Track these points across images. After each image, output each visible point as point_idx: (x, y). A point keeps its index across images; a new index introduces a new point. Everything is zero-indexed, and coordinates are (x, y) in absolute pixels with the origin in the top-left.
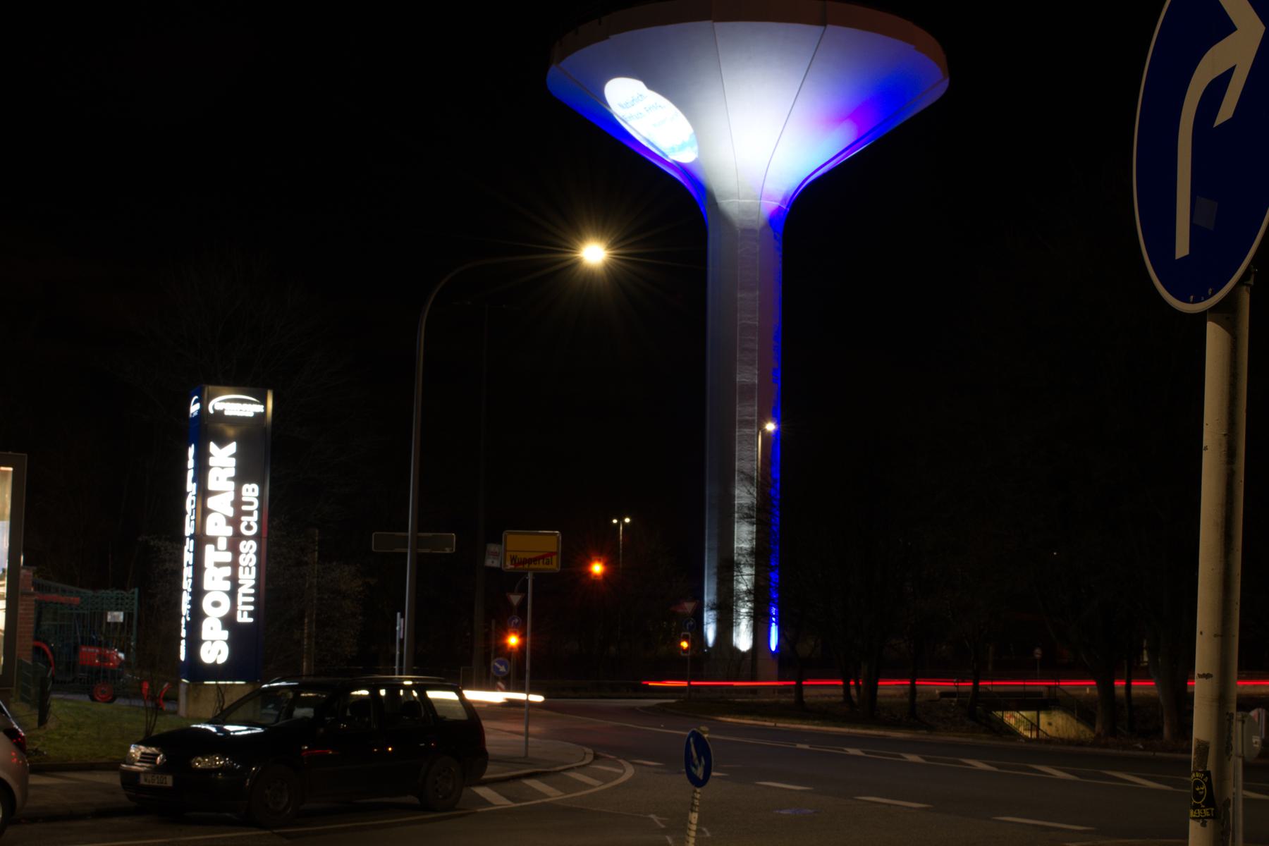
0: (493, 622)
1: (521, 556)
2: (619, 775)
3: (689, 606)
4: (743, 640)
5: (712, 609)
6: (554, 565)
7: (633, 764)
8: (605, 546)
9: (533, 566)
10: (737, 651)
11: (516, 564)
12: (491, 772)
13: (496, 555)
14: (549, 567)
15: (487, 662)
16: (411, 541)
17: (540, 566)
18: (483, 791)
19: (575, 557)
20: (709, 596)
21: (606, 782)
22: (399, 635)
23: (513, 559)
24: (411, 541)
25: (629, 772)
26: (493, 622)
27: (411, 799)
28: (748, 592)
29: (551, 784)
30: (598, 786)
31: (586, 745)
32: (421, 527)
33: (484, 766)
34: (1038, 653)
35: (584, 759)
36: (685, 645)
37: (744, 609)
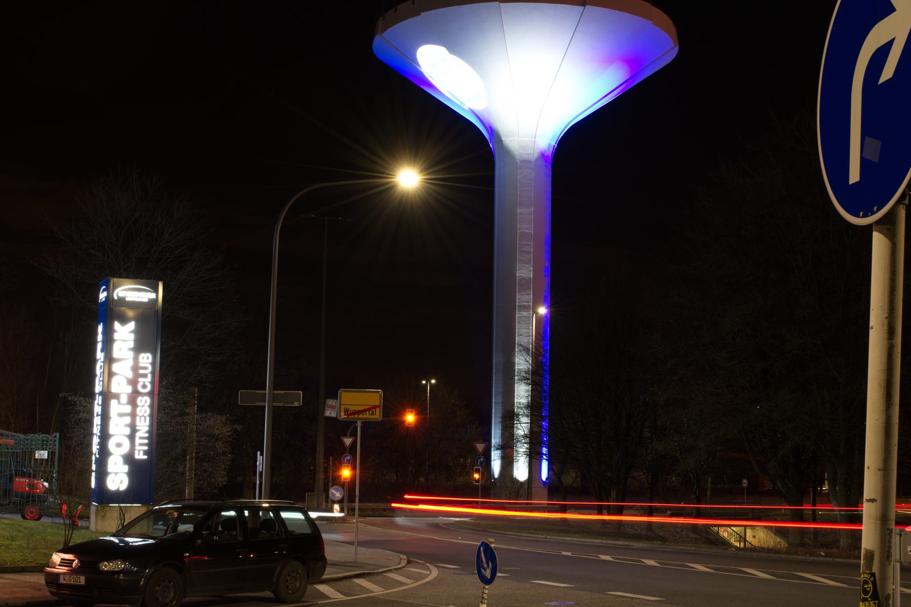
1: (352, 408)
2: (428, 575)
3: (480, 447)
4: (521, 472)
6: (378, 416)
7: (438, 567)
8: (417, 402)
9: (361, 416)
13: (332, 407)
15: (326, 491)
16: (268, 398)
17: (367, 416)
18: (323, 588)
19: (392, 409)
23: (346, 411)
25: (434, 573)
26: (331, 458)
27: (268, 594)
28: (525, 436)
29: (375, 583)
30: (411, 584)
32: (276, 386)
33: (324, 568)
34: (745, 482)
36: (476, 476)
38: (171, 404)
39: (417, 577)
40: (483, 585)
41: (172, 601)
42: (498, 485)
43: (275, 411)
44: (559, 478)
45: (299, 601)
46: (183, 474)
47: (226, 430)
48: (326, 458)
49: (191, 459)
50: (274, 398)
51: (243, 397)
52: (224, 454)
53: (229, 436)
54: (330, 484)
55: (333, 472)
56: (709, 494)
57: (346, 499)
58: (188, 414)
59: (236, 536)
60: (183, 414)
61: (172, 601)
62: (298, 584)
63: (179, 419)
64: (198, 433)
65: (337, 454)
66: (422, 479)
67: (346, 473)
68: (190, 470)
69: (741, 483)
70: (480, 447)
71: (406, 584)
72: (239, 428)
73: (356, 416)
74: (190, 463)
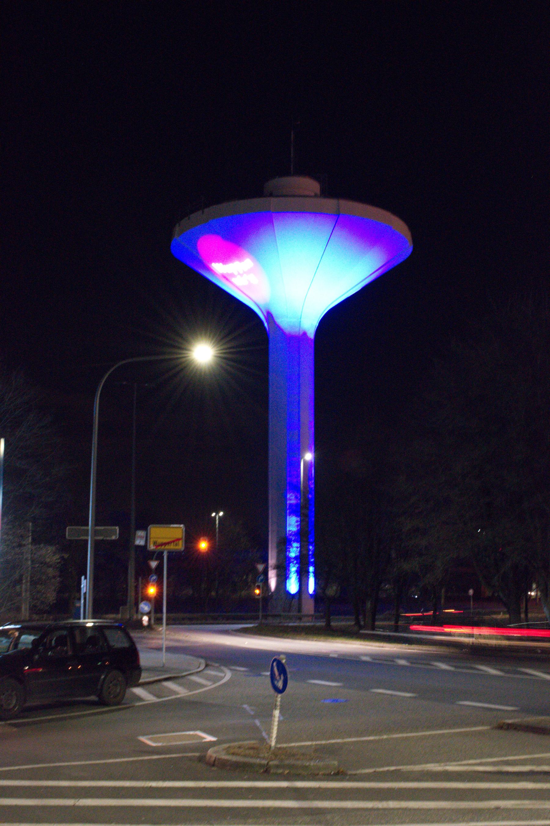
0: (140, 579)
1: (160, 541)
2: (222, 678)
3: (260, 567)
4: (293, 586)
5: (274, 569)
6: (181, 546)
7: (231, 670)
8: (207, 529)
9: (167, 547)
10: (288, 592)
11: (157, 546)
12: (145, 677)
13: (141, 537)
14: (177, 547)
15: (137, 604)
16: (91, 532)
17: (172, 547)
18: (138, 691)
19: (191, 539)
20: (272, 561)
21: (214, 682)
22: (83, 590)
23: (155, 543)
24: (91, 532)
25: (227, 675)
26: (140, 579)
27: (93, 698)
28: (296, 558)
29: (181, 685)
30: (210, 686)
31: (202, 657)
32: (97, 522)
33: (139, 675)
34: (471, 592)
35: (199, 667)
36: (257, 591)
37: (293, 569)
38: (11, 537)
39: (215, 679)
40: (276, 694)
41: (14, 707)
42: (274, 597)
43: (97, 545)
44: (324, 589)
45: (119, 703)
46: (19, 594)
47: (56, 558)
48: (137, 580)
49: (27, 582)
50: (96, 533)
51: (70, 532)
52: (54, 577)
53: (58, 563)
54: (140, 601)
55: (143, 588)
56: (443, 601)
57: (153, 611)
58: (24, 545)
59: (67, 652)
60: (20, 546)
61: (14, 707)
62: (118, 690)
63: (17, 550)
64: (33, 561)
65: (144, 574)
66: (213, 593)
67: (152, 591)
68: (26, 591)
69: (468, 592)
70: (260, 567)
71: (204, 686)
72: (66, 556)
73: (163, 547)
74: (25, 585)
